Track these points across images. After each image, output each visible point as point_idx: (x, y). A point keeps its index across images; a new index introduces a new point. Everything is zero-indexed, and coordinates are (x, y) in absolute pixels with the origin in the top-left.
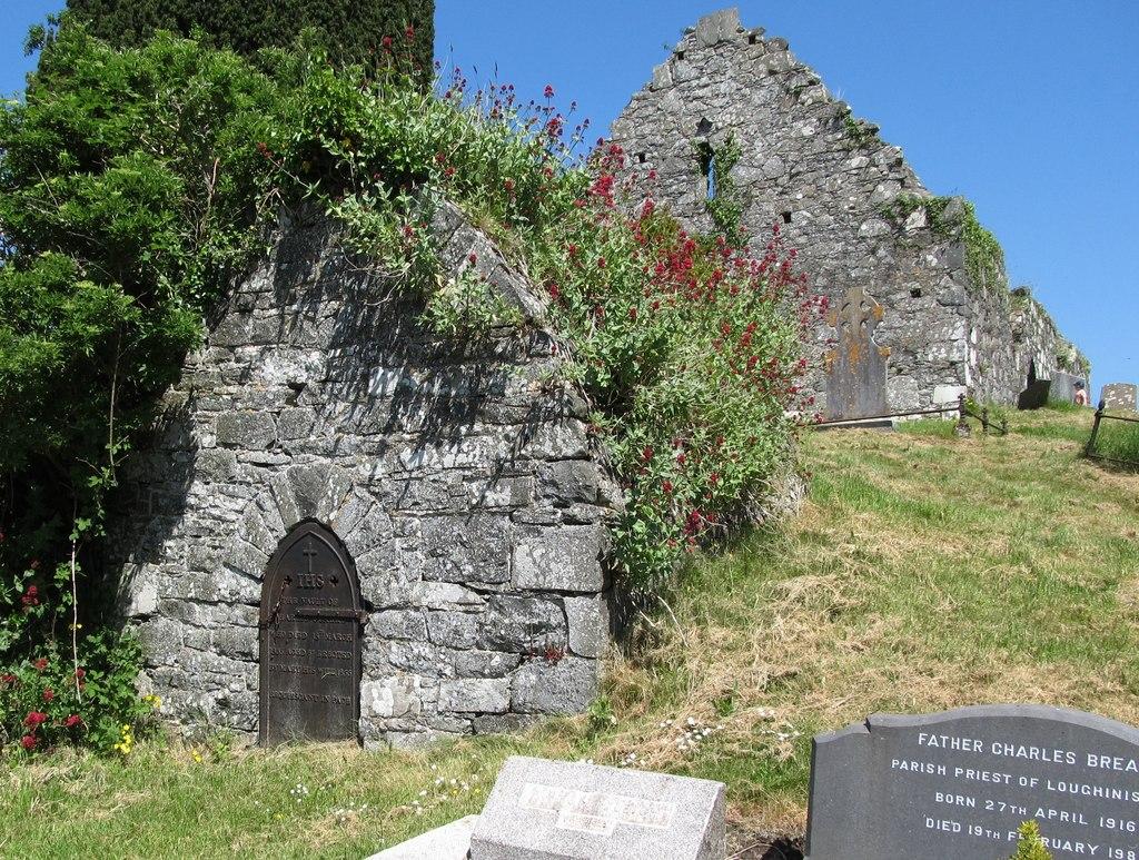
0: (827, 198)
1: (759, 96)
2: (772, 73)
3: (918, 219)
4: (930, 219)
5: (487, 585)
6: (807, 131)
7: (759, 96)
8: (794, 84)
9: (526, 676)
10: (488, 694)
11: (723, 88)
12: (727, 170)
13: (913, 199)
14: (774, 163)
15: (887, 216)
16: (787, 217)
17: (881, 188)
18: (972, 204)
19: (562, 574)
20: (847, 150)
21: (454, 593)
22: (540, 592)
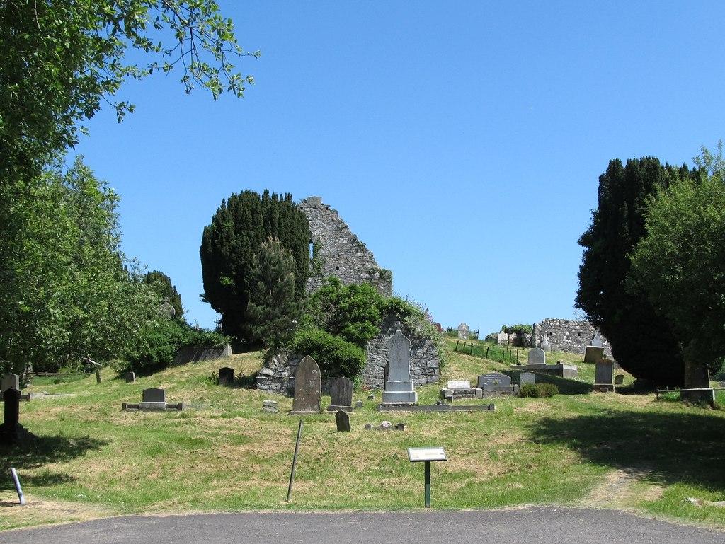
0: (350, 264)
1: (329, 228)
2: (333, 221)
3: (377, 275)
4: (381, 275)
5: (424, 367)
6: (345, 242)
7: (329, 228)
8: (340, 226)
9: (429, 378)
10: (424, 381)
11: (316, 222)
12: (318, 250)
13: (377, 268)
14: (333, 250)
15: (369, 273)
16: (338, 268)
17: (367, 264)
18: (450, 326)
19: (434, 366)
20: (357, 250)
21: (418, 368)
22: (431, 368)
